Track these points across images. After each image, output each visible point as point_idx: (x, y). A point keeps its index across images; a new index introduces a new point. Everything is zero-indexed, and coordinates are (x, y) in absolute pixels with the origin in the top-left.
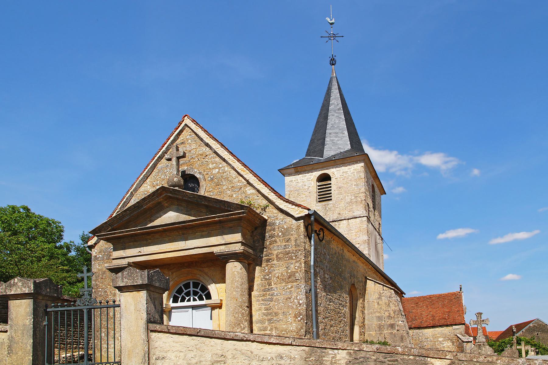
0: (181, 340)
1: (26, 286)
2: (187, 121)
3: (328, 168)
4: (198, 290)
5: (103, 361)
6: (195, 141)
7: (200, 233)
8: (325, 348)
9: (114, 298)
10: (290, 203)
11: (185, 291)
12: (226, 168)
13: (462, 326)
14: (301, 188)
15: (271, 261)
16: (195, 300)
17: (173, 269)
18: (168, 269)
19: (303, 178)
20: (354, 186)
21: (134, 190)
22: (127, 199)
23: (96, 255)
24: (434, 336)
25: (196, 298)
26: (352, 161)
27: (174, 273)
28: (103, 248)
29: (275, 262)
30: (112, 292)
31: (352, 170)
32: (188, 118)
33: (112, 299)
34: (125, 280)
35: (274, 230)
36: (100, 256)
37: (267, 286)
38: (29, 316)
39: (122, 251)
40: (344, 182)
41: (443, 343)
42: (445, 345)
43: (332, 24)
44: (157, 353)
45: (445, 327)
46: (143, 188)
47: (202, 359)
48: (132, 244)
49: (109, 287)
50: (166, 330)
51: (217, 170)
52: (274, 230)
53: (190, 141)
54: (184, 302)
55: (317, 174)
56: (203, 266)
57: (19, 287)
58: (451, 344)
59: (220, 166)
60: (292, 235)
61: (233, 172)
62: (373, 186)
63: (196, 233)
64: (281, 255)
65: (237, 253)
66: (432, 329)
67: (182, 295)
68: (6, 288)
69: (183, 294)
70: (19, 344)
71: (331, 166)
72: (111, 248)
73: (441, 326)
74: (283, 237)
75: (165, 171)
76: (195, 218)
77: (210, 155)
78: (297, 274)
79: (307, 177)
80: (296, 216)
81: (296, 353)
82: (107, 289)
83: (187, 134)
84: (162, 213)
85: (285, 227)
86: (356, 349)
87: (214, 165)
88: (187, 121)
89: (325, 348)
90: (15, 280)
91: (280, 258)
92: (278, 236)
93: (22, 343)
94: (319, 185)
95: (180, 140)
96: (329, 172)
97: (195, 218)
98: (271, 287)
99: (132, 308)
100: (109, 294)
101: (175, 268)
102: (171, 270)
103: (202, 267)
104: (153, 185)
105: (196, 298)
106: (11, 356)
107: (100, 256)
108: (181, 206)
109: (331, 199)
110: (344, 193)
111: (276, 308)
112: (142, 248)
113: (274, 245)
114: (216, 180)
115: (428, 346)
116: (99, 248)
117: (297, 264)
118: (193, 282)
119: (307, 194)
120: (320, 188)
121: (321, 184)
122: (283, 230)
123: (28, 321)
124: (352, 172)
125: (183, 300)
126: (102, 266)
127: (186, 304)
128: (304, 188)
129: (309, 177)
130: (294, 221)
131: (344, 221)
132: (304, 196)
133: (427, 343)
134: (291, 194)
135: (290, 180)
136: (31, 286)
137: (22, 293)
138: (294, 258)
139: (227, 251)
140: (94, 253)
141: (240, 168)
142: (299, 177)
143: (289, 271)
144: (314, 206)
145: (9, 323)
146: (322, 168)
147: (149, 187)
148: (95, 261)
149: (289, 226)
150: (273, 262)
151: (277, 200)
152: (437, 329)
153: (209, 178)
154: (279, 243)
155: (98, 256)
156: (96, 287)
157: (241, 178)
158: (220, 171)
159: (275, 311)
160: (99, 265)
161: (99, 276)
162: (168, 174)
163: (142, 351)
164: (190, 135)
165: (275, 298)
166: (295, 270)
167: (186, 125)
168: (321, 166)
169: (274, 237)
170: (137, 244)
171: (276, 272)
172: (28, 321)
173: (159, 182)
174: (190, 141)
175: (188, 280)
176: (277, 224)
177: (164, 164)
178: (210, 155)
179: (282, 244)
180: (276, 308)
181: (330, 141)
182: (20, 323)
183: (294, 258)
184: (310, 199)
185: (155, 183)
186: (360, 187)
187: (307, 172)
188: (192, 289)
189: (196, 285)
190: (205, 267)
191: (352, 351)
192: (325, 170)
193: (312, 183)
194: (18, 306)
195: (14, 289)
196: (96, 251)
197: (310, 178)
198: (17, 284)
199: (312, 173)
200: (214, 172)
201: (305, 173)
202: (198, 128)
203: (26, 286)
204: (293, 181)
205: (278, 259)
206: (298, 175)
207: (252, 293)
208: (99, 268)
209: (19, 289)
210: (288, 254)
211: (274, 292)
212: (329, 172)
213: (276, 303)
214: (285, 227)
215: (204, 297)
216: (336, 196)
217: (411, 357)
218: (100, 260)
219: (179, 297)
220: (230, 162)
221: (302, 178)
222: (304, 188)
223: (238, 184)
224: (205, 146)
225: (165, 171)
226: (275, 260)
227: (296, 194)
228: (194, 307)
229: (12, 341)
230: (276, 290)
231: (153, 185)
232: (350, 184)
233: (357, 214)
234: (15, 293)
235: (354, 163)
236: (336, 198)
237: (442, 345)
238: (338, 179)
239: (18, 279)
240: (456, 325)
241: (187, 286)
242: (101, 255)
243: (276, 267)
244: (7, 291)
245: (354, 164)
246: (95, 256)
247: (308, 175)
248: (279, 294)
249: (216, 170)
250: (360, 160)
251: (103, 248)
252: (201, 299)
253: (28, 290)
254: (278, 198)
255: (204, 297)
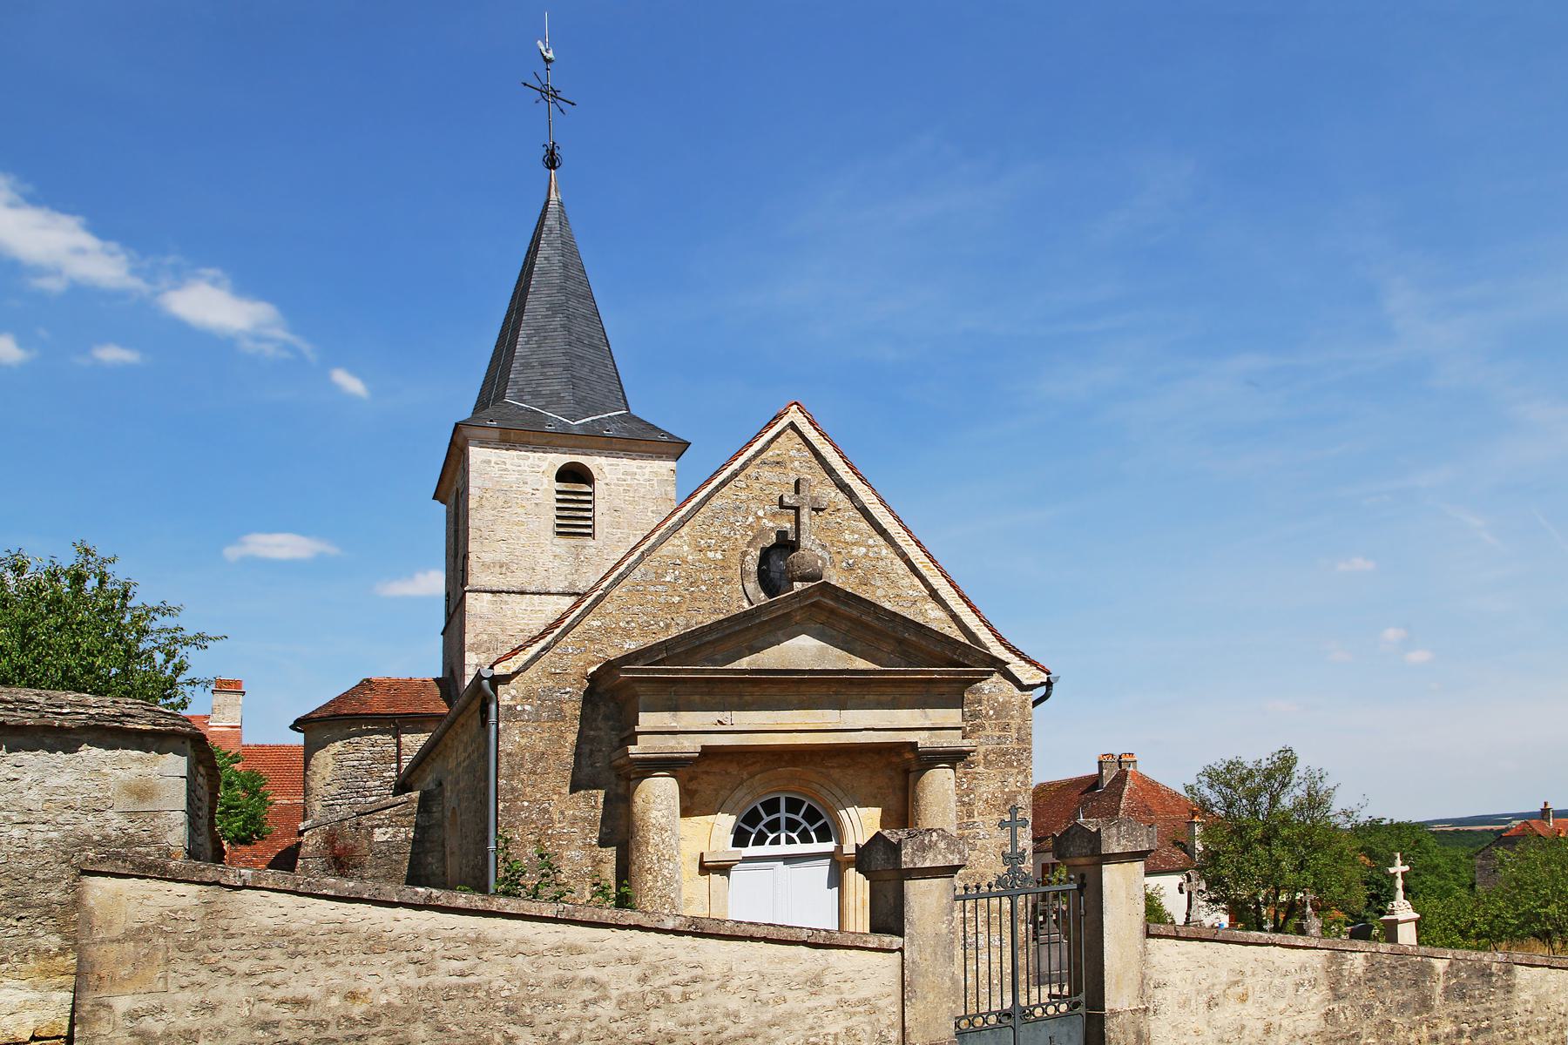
0: (1189, 950)
1: (954, 850)
2: (795, 416)
3: (588, 451)
4: (799, 818)
5: (1042, 1002)
6: (811, 468)
7: (876, 697)
8: (1345, 951)
9: (572, 830)
10: (1016, 655)
11: (767, 819)
12: (884, 552)
14: (514, 488)
15: (972, 766)
16: (790, 841)
17: (751, 765)
18: (738, 764)
19: (521, 461)
21: (648, 550)
22: (629, 565)
23: (512, 703)
25: (794, 835)
27: (758, 777)
28: (537, 686)
29: (981, 769)
30: (566, 813)
31: (647, 471)
32: (801, 411)
33: (565, 831)
34: (1123, 842)
35: (980, 702)
36: (528, 708)
37: (966, 817)
38: (947, 915)
39: (666, 714)
40: (627, 498)
43: (548, 61)
44: (1155, 977)
46: (670, 548)
47: (1216, 981)
48: (697, 698)
49: (555, 797)
50: (1174, 934)
51: (863, 550)
52: (980, 702)
53: (797, 463)
54: (763, 844)
56: (830, 765)
57: (940, 852)
59: (871, 542)
60: (1012, 717)
61: (899, 562)
63: (867, 697)
64: (992, 755)
65: (964, 751)
67: (757, 829)
68: (913, 853)
69: (761, 826)
70: (927, 977)
71: (596, 448)
72: (563, 691)
74: (996, 719)
75: (732, 520)
76: (880, 668)
77: (846, 510)
78: (1020, 798)
79: (531, 460)
80: (1026, 682)
81: (1317, 959)
82: (549, 804)
83: (790, 444)
84: (783, 634)
85: (1001, 700)
86: (1374, 950)
87: (856, 536)
88: (795, 416)
89: (1345, 951)
90: (931, 836)
91: (990, 762)
92: (987, 716)
93: (933, 974)
94: (560, 489)
95: (771, 454)
96: (593, 462)
97: (880, 668)
98: (973, 820)
99: (1123, 894)
100: (555, 817)
101: (758, 762)
102: (746, 766)
103: (827, 767)
104: (698, 546)
105: (794, 835)
106: (913, 1004)
107: (528, 708)
108: (832, 627)
110: (626, 525)
111: (983, 864)
112: (728, 714)
113: (980, 733)
114: (859, 571)
116: (523, 687)
117: (1020, 778)
118: (786, 798)
119: (530, 506)
120: (563, 499)
121: (565, 489)
122: (996, 704)
123: (944, 926)
124: (646, 477)
125: (760, 841)
126: (533, 737)
127: (766, 849)
128: (520, 489)
129: (537, 462)
130: (1016, 691)
132: (520, 511)
134: (487, 499)
135: (484, 458)
136: (964, 851)
137: (947, 864)
138: (1015, 764)
139: (945, 745)
140: (507, 697)
141: (920, 560)
142: (511, 457)
143: (1007, 790)
144: (547, 542)
145: (907, 931)
146: (572, 449)
147: (686, 548)
148: (510, 721)
149: (1007, 699)
150: (976, 769)
151: (993, 644)
153: (844, 564)
154: (989, 732)
155: (519, 708)
156: (512, 797)
157: (917, 581)
158: (871, 554)
159: (981, 870)
160: (523, 734)
161: (522, 766)
162: (739, 528)
163: (1139, 974)
164: (799, 450)
165: (979, 843)
166: (1016, 789)
167: (792, 426)
168: (571, 443)
169: (979, 718)
170: (713, 701)
171: (983, 789)
172: (944, 926)
173: (713, 541)
174: (797, 463)
175: (776, 791)
176: (987, 692)
177: (730, 501)
178: (846, 510)
179: (994, 734)
180: (983, 864)
181: (565, 372)
182: (930, 931)
183: (1015, 764)
184: (537, 524)
185: (703, 542)
187: (530, 448)
188: (783, 815)
189: (794, 806)
190: (832, 767)
191: (1369, 954)
192: (578, 454)
193: (545, 480)
194: (924, 894)
195: (931, 855)
196: (513, 692)
197: (539, 467)
198: (935, 844)
199: (543, 452)
200: (854, 552)
201: (526, 449)
202: (824, 443)
203: (954, 850)
204: (493, 464)
205: (988, 764)
206: (507, 450)
207: (85, 746)
208: (523, 742)
209: (940, 857)
210: (1004, 755)
211: (978, 830)
212: (593, 462)
213: (983, 854)
214: (1001, 700)
215: (813, 834)
216: (606, 530)
217: (1419, 958)
218: (528, 721)
219: (752, 834)
220: (899, 541)
221: (516, 460)
222: (520, 489)
223: (911, 592)
224: (834, 488)
225: (732, 520)
226: (982, 765)
227: (500, 503)
228: (788, 859)
229: (913, 970)
230: (982, 827)
231: (698, 546)
232: (642, 507)
234: (933, 865)
235: (652, 457)
236: (605, 534)
238: (613, 487)
239: (938, 834)
241: (771, 806)
242: (532, 705)
243: (983, 780)
244: (916, 860)
245: (651, 458)
246: (509, 708)
247: (534, 457)
248: (987, 837)
249: (861, 548)
250: (667, 453)
251: (537, 686)
252: (806, 838)
253: (959, 859)
254: (995, 640)
255: (813, 834)
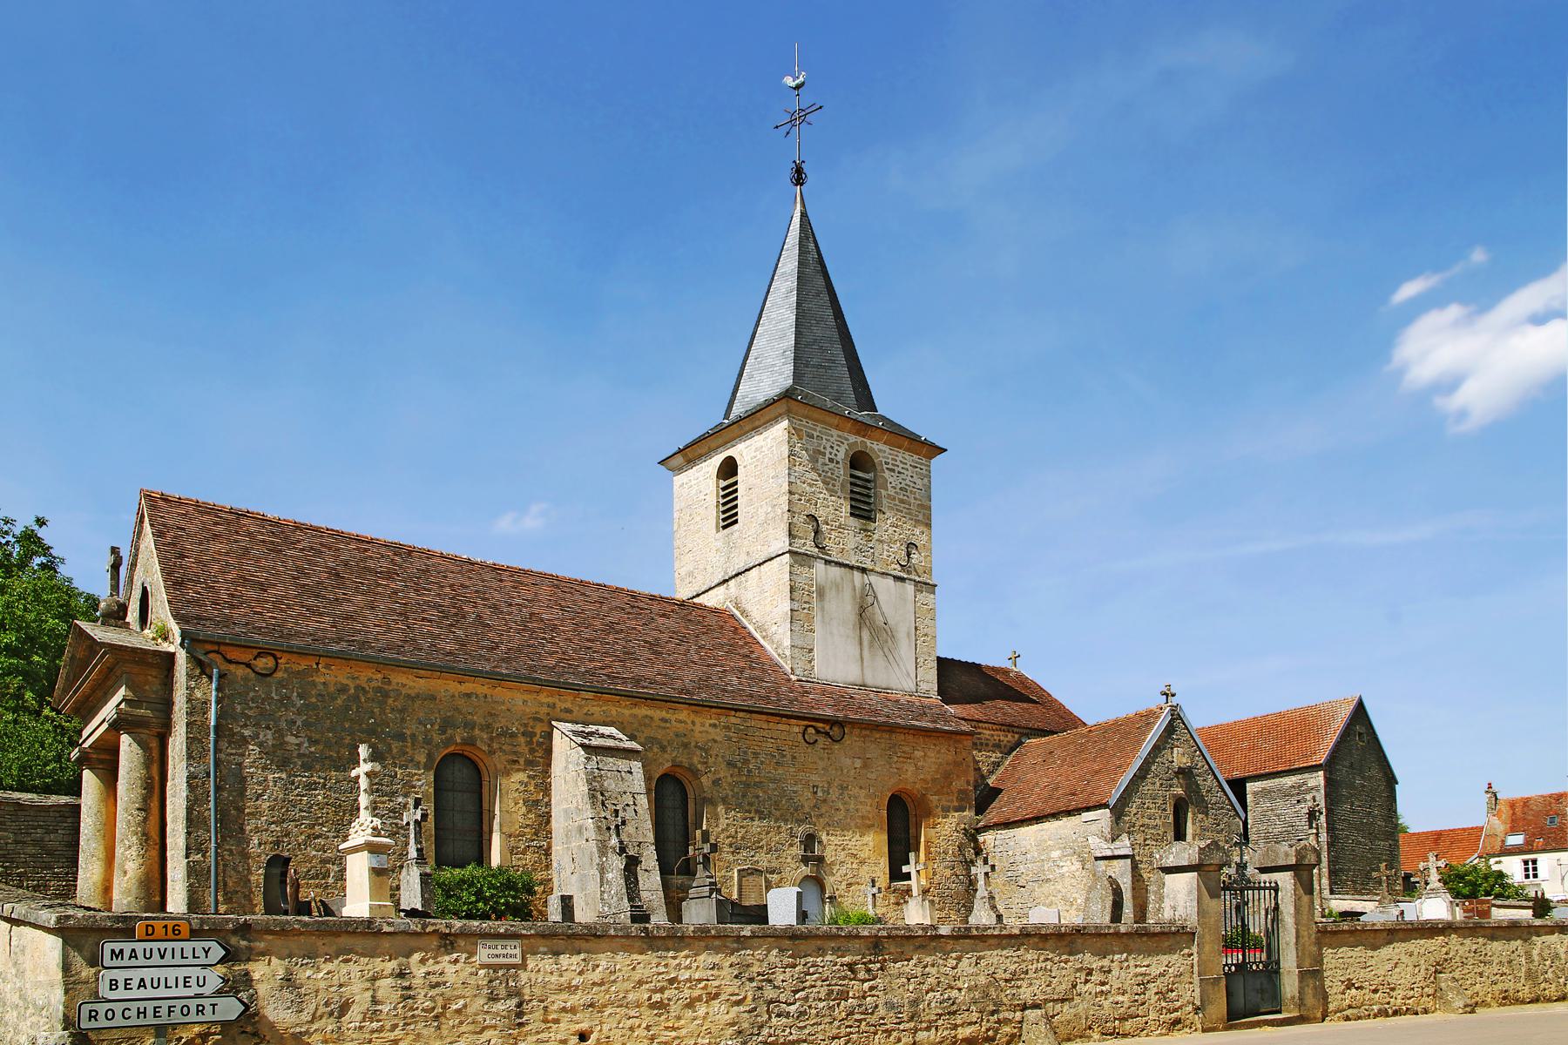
13: (1103, 810)
20: (771, 480)
24: (1043, 848)
26: (768, 418)
41: (1061, 864)
42: (1065, 869)
43: (798, 87)
45: (1065, 819)
55: (717, 460)
58: (1078, 865)
62: (143, 516)
66: (1035, 827)
73: (1055, 816)
109: (736, 522)
115: (1027, 875)
131: (754, 569)
133: (1025, 868)
152: (1046, 825)
168: (720, 441)
186: (780, 481)
221: (697, 475)
233: (773, 551)
237: (1057, 871)
240: (1088, 809)
